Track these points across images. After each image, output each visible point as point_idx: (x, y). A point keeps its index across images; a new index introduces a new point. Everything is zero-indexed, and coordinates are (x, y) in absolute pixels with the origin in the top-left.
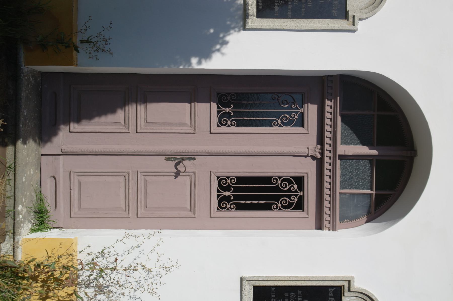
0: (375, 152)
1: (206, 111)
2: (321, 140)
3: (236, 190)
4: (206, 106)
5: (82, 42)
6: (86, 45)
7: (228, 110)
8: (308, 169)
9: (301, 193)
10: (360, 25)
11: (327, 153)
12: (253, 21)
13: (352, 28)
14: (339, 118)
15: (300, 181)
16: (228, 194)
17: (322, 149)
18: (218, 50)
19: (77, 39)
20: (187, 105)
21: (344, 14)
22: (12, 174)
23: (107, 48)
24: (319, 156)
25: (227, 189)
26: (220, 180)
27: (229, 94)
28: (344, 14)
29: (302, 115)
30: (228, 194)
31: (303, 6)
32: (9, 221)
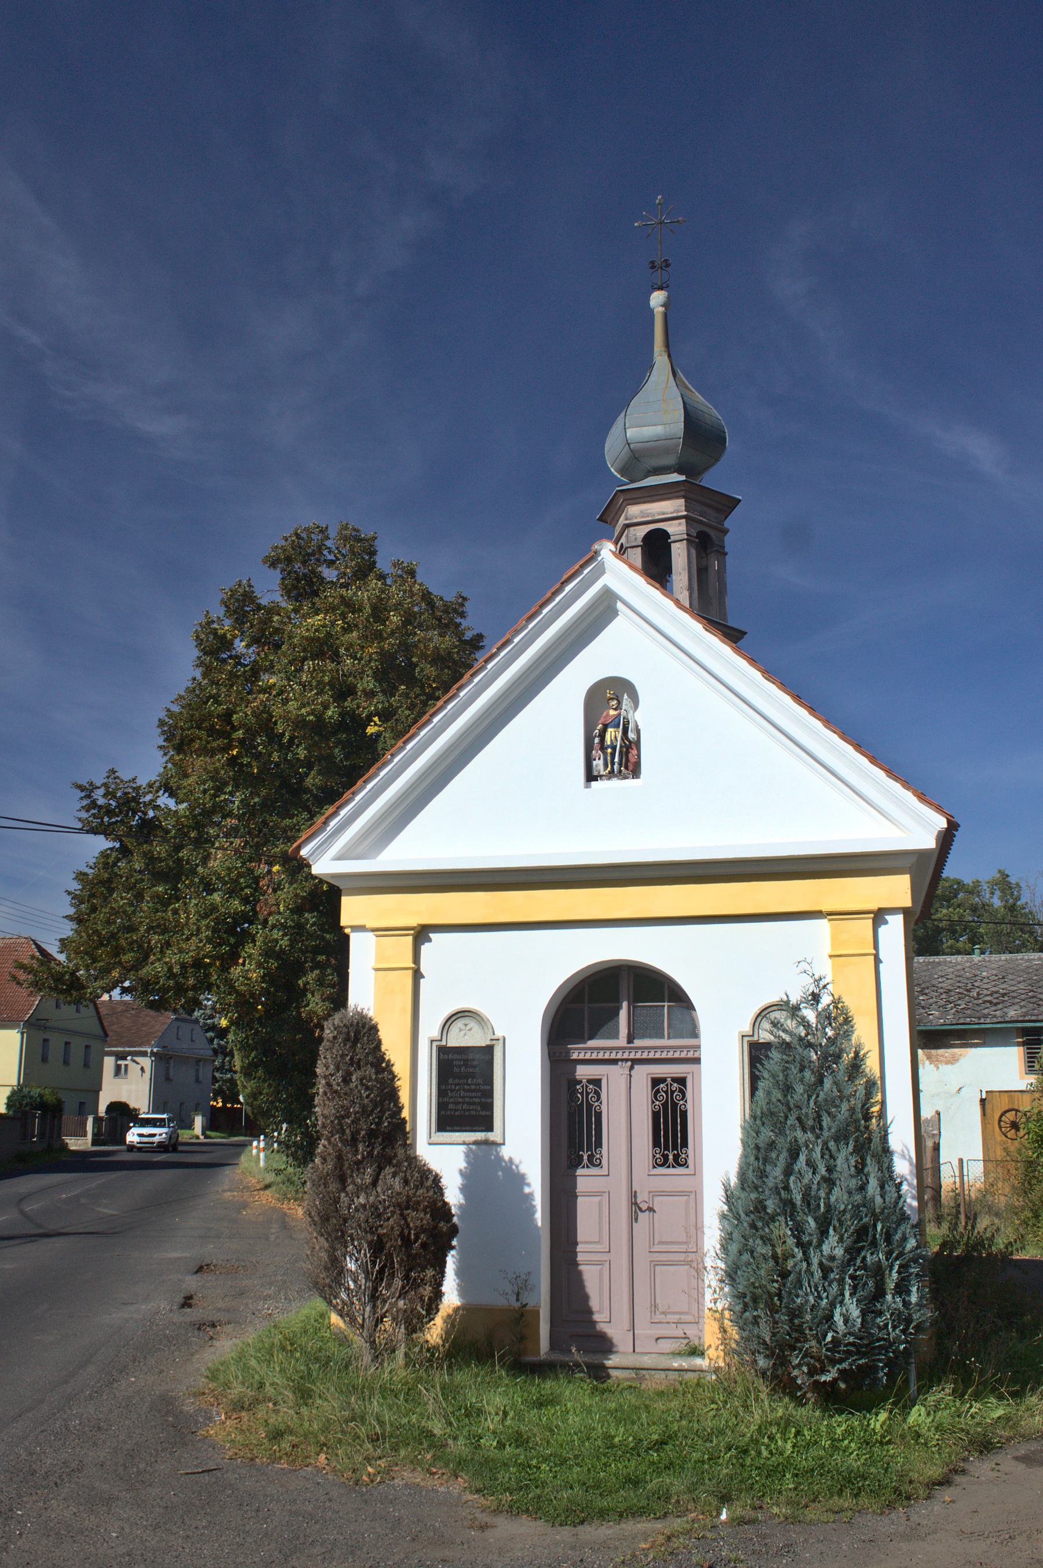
0: (625, 1004)
1: (585, 1180)
2: (614, 1062)
3: (666, 1148)
4: (579, 1180)
5: (517, 1300)
6: (521, 1296)
7: (585, 1157)
8: (643, 1074)
9: (669, 1080)
10: (499, 1034)
11: (626, 1056)
12: (491, 1136)
13: (501, 1041)
14: (591, 1043)
15: (656, 1082)
16: (671, 1157)
17: (622, 1060)
18: (517, 1167)
19: (517, 1305)
20: (579, 1199)
21: (489, 1050)
22: (644, 1372)
23: (523, 1277)
24: (629, 1063)
25: (666, 1157)
26: (656, 1165)
27: (569, 1157)
28: (489, 1050)
29: (590, 1081)
30: (671, 1157)
31: (482, 1087)
32: (689, 1376)
